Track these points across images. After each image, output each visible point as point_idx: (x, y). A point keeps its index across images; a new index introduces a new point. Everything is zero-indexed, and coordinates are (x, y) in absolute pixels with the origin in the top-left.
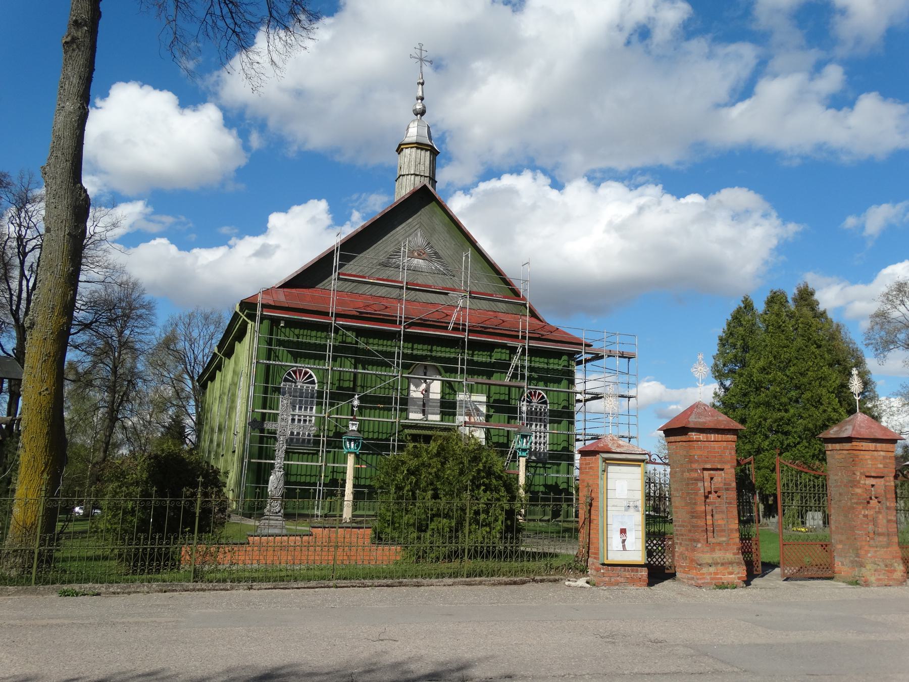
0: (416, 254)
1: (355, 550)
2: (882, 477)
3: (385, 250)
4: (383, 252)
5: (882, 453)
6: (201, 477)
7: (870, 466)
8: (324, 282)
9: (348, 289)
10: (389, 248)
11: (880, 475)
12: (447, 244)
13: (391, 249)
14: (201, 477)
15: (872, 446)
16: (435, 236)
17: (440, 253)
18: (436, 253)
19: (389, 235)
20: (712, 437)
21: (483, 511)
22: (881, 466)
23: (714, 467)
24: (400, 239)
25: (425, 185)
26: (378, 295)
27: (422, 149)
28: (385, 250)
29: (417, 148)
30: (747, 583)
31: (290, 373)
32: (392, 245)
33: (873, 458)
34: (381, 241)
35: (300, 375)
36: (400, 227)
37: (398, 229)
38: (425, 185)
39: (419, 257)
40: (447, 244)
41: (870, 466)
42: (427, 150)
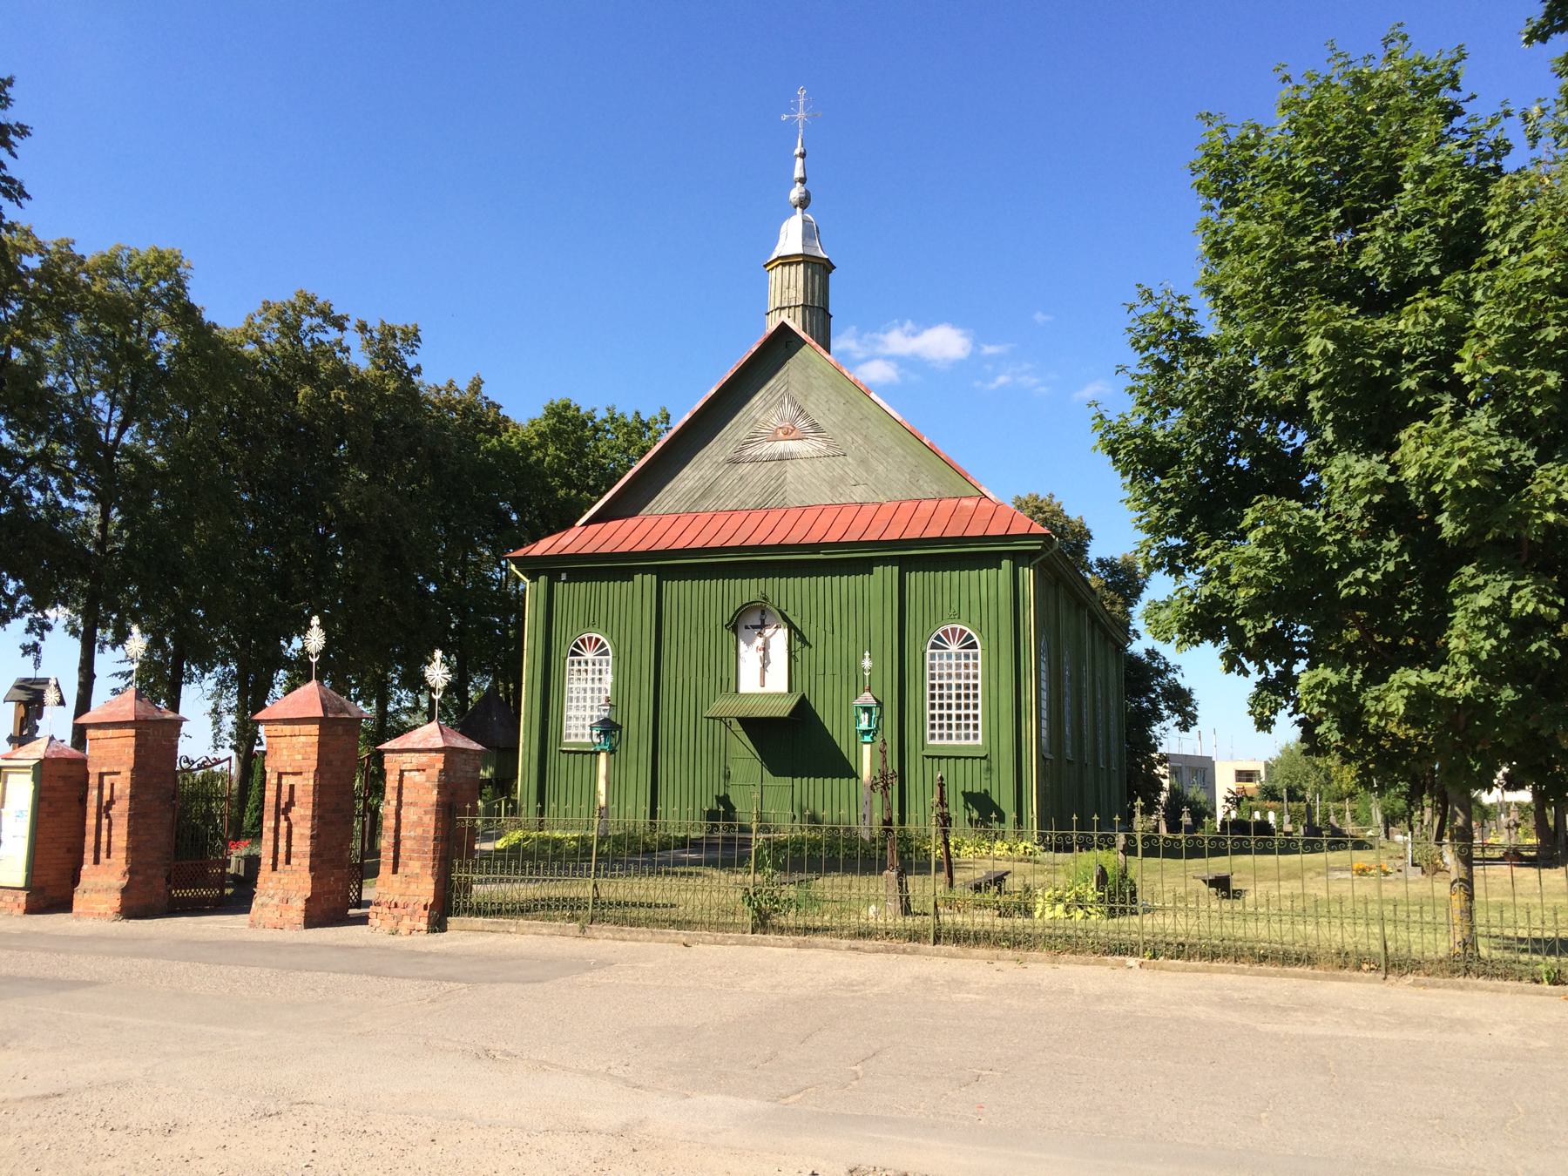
0: (781, 434)
1: (1338, 924)
2: (300, 773)
3: (736, 438)
4: (732, 441)
5: (302, 739)
6: (1139, 799)
7: (286, 758)
8: (650, 505)
9: (684, 509)
10: (740, 433)
11: (296, 770)
12: (832, 405)
13: (743, 434)
14: (1139, 799)
15: (287, 729)
16: (812, 398)
17: (821, 422)
18: (814, 425)
19: (740, 414)
20: (110, 733)
21: (1195, 839)
22: (299, 757)
23: (111, 770)
24: (757, 416)
25: (783, 323)
26: (727, 509)
27: (790, 264)
28: (736, 438)
29: (784, 265)
30: (438, 924)
31: (572, 651)
32: (746, 428)
33: (291, 747)
34: (729, 425)
35: (590, 645)
36: (756, 398)
37: (753, 401)
38: (783, 323)
39: (787, 437)
40: (832, 405)
41: (286, 758)
42: (798, 263)
